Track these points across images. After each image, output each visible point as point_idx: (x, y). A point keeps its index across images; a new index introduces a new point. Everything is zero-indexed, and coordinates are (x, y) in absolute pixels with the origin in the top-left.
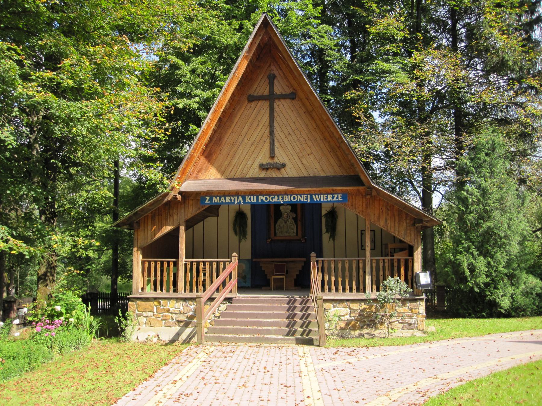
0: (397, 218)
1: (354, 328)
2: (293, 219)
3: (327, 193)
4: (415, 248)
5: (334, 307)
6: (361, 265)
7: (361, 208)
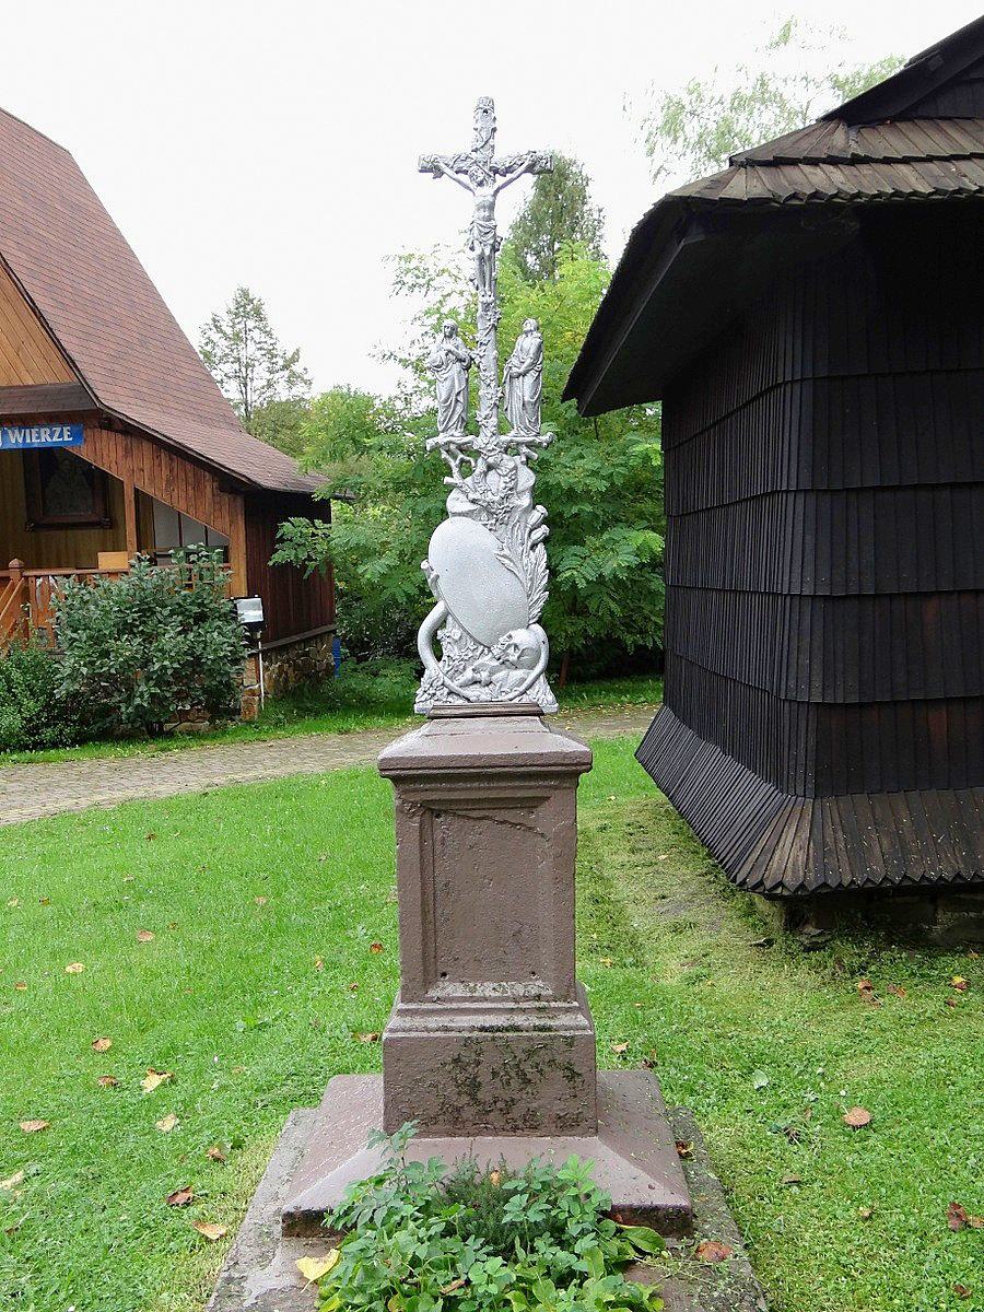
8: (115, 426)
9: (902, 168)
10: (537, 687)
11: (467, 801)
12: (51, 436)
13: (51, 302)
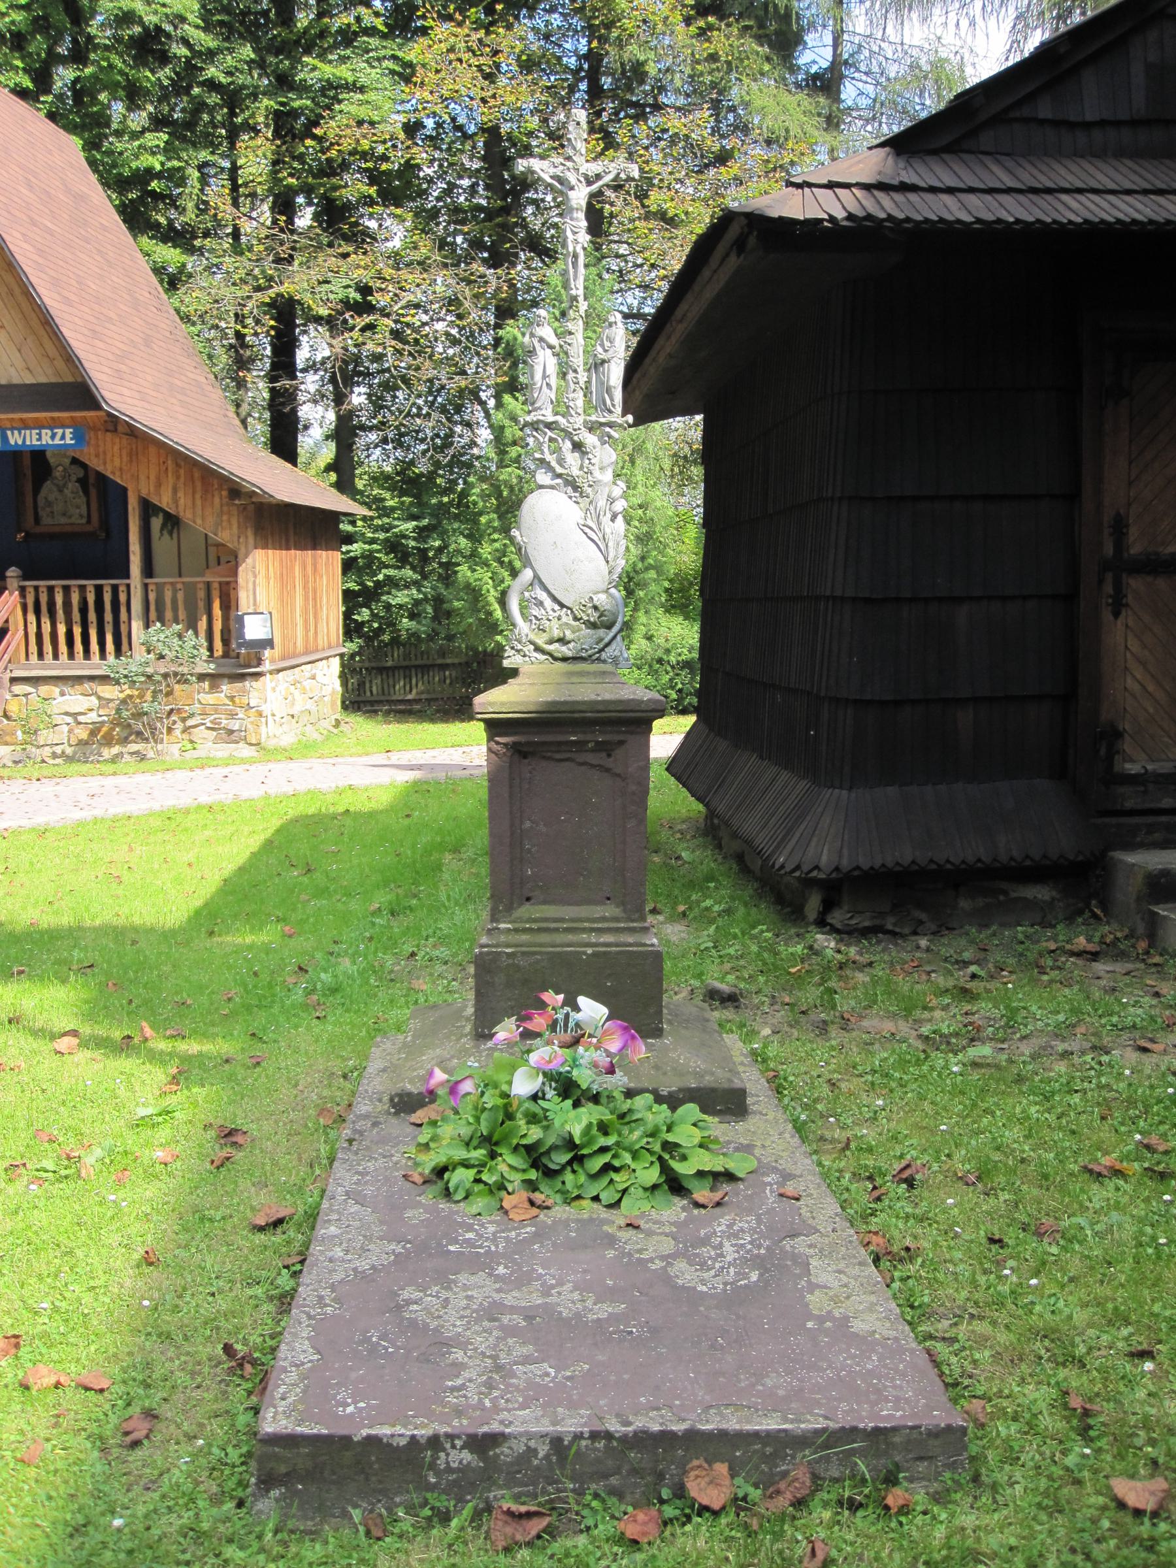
0: (199, 484)
1: (108, 741)
2: (79, 480)
3: (39, 425)
4: (240, 556)
5: (62, 694)
6: (123, 597)
7: (117, 463)
8: (120, 428)
9: (945, 198)
10: (614, 645)
11: (551, 743)
12: (53, 437)
13: (56, 296)
